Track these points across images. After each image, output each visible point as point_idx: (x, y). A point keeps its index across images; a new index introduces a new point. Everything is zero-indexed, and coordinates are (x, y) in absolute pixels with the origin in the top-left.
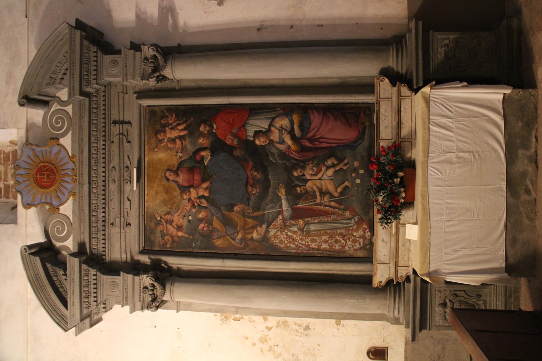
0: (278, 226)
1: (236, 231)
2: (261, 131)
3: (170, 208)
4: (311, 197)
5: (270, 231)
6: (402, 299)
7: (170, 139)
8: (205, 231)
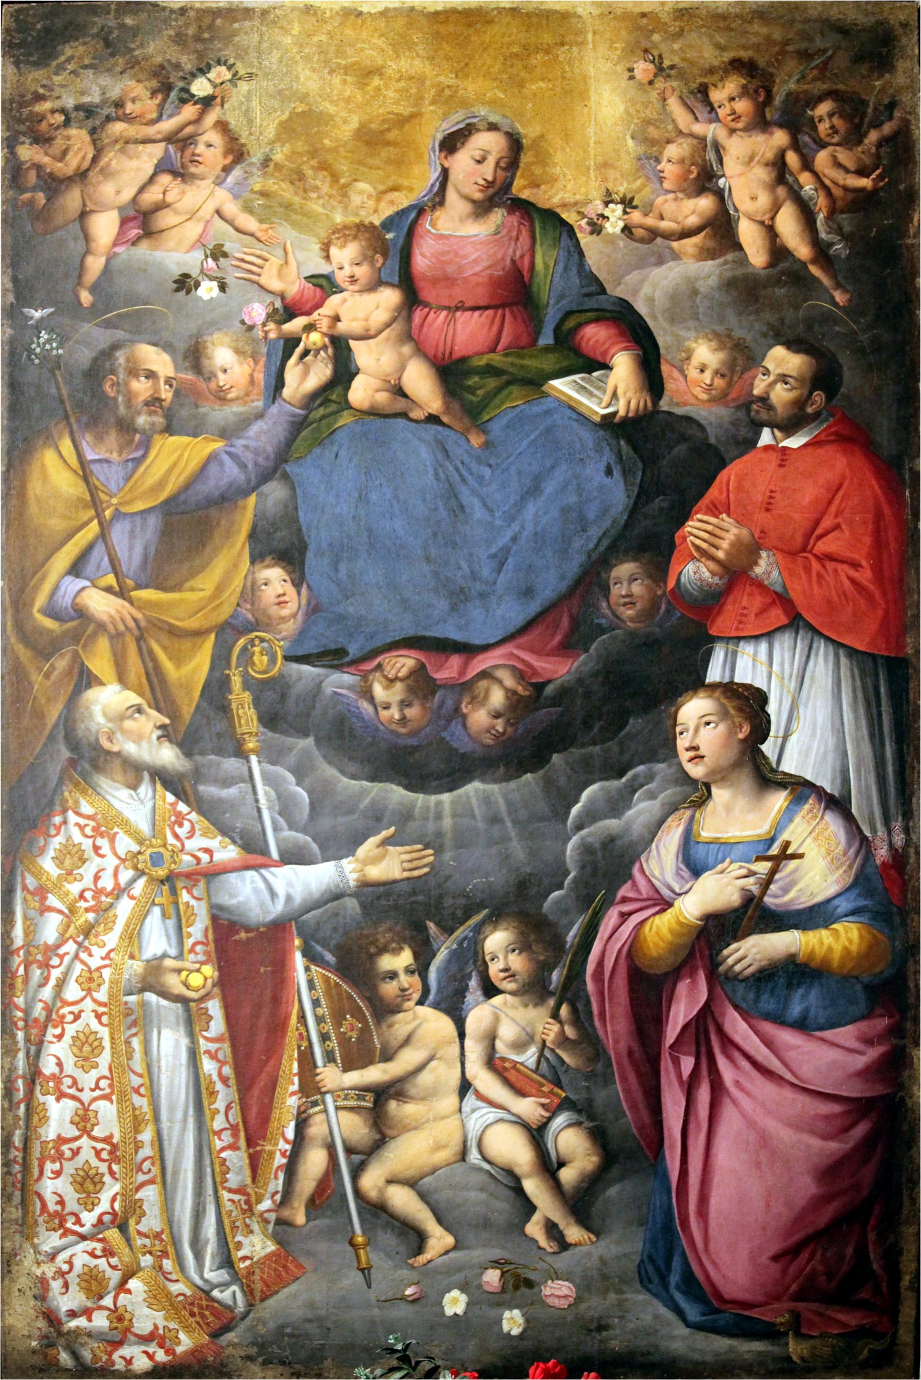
0: (171, 840)
1: (130, 583)
2: (761, 730)
3: (266, 162)
4: (354, 1035)
5: (134, 787)
6: (414, 855)
7: (711, 155)
8: (127, 384)
